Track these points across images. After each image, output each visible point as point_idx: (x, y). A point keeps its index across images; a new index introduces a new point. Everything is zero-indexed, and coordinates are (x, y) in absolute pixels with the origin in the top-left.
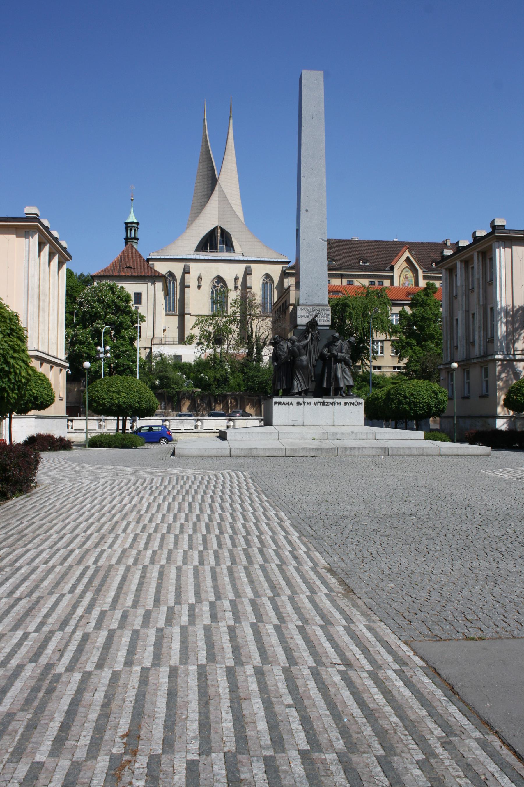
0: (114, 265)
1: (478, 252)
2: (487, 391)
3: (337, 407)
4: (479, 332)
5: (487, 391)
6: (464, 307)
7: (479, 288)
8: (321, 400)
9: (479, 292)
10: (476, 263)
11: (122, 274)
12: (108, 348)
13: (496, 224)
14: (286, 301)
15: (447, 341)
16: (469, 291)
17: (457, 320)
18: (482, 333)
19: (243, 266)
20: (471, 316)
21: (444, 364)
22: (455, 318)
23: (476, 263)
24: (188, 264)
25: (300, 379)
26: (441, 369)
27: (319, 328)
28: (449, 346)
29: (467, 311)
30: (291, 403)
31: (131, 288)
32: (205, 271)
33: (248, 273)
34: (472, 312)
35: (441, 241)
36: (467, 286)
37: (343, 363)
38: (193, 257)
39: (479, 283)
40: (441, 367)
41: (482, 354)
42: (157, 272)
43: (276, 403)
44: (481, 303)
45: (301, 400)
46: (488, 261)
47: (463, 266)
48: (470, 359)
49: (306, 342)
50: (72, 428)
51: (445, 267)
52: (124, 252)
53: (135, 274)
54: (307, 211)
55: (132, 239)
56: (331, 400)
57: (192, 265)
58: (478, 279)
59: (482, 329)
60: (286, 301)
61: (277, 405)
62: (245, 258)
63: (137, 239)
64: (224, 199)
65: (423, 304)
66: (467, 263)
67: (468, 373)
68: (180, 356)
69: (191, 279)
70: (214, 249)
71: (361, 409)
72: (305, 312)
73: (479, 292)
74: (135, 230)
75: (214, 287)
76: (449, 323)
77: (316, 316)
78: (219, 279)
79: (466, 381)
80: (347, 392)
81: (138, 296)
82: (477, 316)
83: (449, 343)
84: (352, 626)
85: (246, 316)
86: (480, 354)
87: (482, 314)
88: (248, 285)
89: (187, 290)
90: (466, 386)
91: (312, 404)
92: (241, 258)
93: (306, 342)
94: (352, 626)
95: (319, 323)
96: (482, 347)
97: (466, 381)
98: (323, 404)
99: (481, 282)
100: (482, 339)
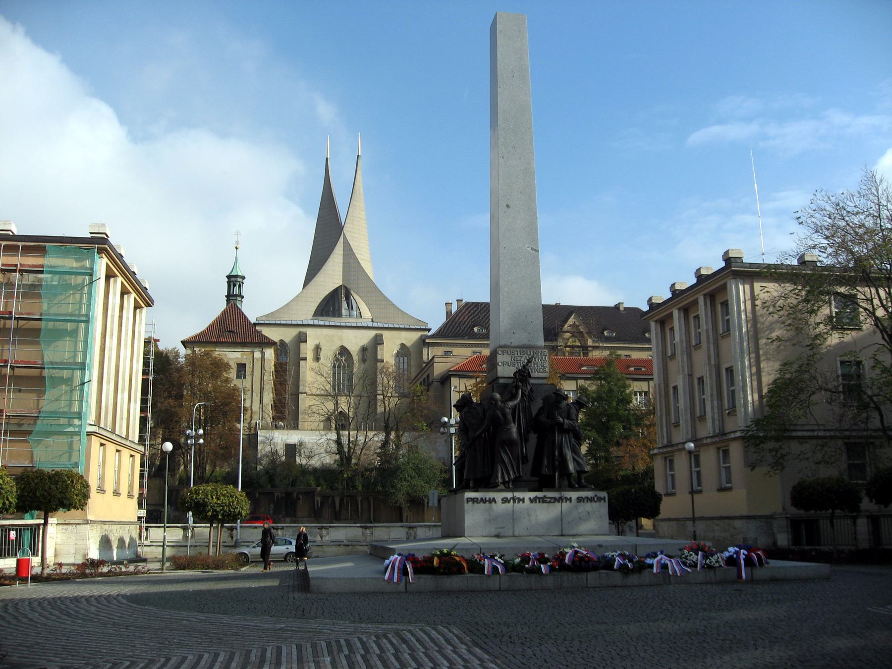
0: (211, 328)
1: (705, 295)
2: (673, 487)
3: (566, 505)
4: (712, 402)
5: (699, 484)
6: (686, 369)
7: (708, 342)
8: (540, 494)
9: (708, 348)
10: (702, 309)
11: (222, 339)
12: (201, 432)
13: (731, 255)
14: (428, 376)
15: (661, 416)
16: (690, 349)
17: (675, 388)
18: (715, 403)
19: (372, 333)
20: (671, 391)
21: (659, 448)
22: (672, 385)
23: (702, 309)
24: (303, 330)
25: (506, 460)
26: (655, 454)
27: (532, 381)
28: (664, 424)
29: (691, 375)
30: (494, 499)
31: (233, 356)
32: (326, 340)
33: (378, 341)
34: (697, 375)
35: (612, 305)
36: (688, 341)
37: (571, 435)
38: (311, 322)
39: (708, 337)
40: (656, 451)
41: (717, 431)
42: (266, 337)
43: (468, 500)
44: (713, 362)
45: (509, 495)
46: (719, 307)
47: (682, 315)
48: (725, 434)
49: (515, 402)
50: (147, 538)
51: (656, 318)
52: (224, 313)
53: (239, 340)
54: (508, 206)
55: (236, 295)
56: (556, 495)
57: (310, 332)
58: (707, 331)
59: (715, 398)
60: (428, 376)
61: (470, 503)
62: (375, 325)
63: (243, 297)
64: (349, 252)
65: (607, 377)
66: (686, 311)
67: (671, 461)
68: (403, 345)
69: (307, 350)
70: (337, 313)
71: (602, 509)
72: (509, 357)
73: (708, 348)
74: (240, 286)
75: (337, 360)
76: (663, 393)
77: (529, 361)
78: (344, 351)
79: (722, 465)
80: (577, 482)
81: (241, 367)
82: (707, 381)
83: (664, 419)
84: (352, 655)
85: (376, 396)
86: (714, 431)
87: (714, 378)
88: (379, 357)
89: (302, 363)
90: (670, 478)
91: (527, 500)
92: (370, 324)
93: (515, 402)
94: (352, 655)
95: (532, 375)
96: (717, 423)
97: (669, 473)
98: (543, 500)
99: (711, 334)
100: (716, 410)
